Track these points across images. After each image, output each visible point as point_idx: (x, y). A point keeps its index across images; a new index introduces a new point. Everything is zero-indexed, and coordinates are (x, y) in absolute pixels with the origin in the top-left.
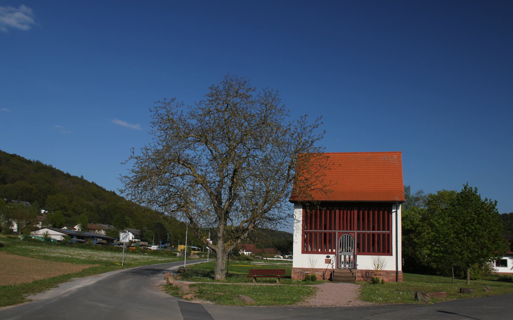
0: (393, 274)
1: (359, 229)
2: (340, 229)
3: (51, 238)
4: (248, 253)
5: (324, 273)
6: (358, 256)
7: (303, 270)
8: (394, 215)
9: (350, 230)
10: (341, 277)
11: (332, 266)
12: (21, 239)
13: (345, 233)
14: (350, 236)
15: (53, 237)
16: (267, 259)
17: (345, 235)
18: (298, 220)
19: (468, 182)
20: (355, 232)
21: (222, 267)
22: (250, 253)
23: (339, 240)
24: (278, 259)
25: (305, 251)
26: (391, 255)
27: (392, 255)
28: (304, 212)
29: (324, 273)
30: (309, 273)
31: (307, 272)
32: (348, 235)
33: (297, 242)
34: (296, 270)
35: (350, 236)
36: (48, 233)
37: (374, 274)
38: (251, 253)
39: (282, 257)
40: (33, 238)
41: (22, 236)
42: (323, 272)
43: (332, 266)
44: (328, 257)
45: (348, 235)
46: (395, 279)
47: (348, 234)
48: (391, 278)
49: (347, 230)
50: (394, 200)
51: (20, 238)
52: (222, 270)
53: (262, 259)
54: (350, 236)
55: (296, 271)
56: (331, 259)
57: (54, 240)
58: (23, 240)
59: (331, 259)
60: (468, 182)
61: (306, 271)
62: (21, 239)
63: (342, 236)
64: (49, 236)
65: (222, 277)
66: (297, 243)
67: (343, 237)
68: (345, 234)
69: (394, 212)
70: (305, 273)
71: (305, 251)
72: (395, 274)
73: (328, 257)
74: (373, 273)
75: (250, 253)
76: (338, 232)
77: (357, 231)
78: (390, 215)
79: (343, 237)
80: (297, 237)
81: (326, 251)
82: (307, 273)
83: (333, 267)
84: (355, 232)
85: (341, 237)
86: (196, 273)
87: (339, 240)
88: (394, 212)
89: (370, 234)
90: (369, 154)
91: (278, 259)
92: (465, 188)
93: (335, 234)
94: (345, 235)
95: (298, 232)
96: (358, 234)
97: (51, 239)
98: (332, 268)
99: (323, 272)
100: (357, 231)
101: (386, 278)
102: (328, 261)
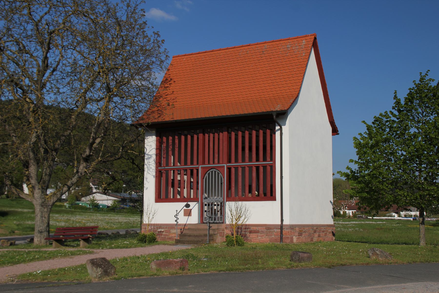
0: (275, 230)
1: (229, 161)
2: (204, 163)
3: (98, 203)
4: (351, 211)
5: (182, 230)
6: (227, 203)
7: (155, 227)
8: (278, 134)
9: (219, 163)
10: (190, 236)
11: (176, 219)
12: (67, 207)
13: (212, 169)
14: (219, 172)
15: (100, 203)
16: (373, 218)
17: (212, 172)
18: (150, 154)
19: (429, 71)
20: (224, 166)
21: (41, 226)
22: (354, 211)
23: (204, 180)
24: (390, 218)
25: (159, 198)
26: (275, 199)
27: (275, 199)
28: (158, 143)
29: (182, 230)
30: (163, 232)
31: (160, 230)
32: (215, 172)
33: (147, 188)
35: (218, 172)
36: (95, 198)
37: (248, 230)
38: (355, 211)
39: (396, 216)
40: (80, 204)
41: (67, 203)
42: (181, 229)
43: (176, 219)
45: (215, 172)
46: (279, 238)
47: (216, 170)
48: (273, 236)
49: (214, 163)
50: (268, 110)
51: (65, 206)
52: (41, 232)
53: (367, 218)
54: (218, 172)
55: (147, 229)
56: (191, 209)
57: (104, 206)
58: (70, 207)
59: (191, 209)
60: (429, 71)
61: (159, 229)
62: (67, 207)
63: (208, 173)
64: (96, 202)
65: (41, 240)
66: (148, 188)
67: (209, 174)
68: (211, 170)
69: (278, 130)
70: (159, 232)
71: (159, 198)
72: (279, 230)
73: (188, 206)
74: (248, 228)
75: (355, 212)
77: (227, 165)
78: (273, 135)
79: (209, 174)
80: (148, 180)
81: (172, 198)
82: (161, 232)
83: (178, 221)
84: (224, 166)
85: (207, 175)
86: (116, 236)
87: (204, 180)
88: (278, 130)
89: (245, 167)
90: (266, 45)
91: (390, 218)
92: (422, 80)
93: (198, 170)
94: (212, 172)
95: (149, 172)
96: (229, 169)
97: (99, 204)
98: (176, 223)
99: (181, 229)
100: (227, 165)
101: (267, 237)
102: (188, 213)
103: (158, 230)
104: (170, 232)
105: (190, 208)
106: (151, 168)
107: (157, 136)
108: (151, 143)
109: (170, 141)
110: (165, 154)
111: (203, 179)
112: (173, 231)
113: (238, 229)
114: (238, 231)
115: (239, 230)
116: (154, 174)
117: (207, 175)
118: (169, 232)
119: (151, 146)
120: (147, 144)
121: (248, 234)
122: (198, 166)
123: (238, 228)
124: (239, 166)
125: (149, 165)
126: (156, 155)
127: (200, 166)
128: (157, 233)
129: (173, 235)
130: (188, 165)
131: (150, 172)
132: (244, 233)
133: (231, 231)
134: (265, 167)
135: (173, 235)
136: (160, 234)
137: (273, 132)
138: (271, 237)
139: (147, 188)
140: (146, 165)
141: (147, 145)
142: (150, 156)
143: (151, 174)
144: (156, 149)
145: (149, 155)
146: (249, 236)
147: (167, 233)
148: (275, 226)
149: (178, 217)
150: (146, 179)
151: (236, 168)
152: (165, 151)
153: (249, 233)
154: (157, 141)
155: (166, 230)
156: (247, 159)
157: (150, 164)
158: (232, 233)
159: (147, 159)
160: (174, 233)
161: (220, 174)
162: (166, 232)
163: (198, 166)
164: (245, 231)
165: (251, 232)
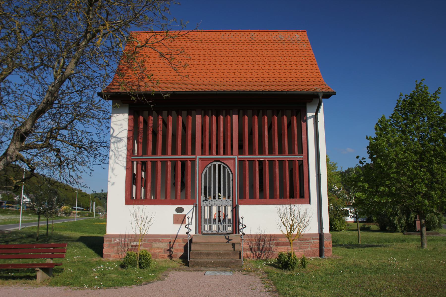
0: (312, 241)
2: (203, 153)
5: (172, 244)
7: (127, 240)
8: (310, 122)
10: (208, 254)
14: (225, 166)
17: (215, 166)
18: (119, 136)
20: (235, 158)
29: (172, 244)
31: (135, 244)
32: (219, 166)
33: (114, 183)
34: (113, 239)
35: (223, 166)
42: (170, 242)
44: (180, 210)
45: (219, 166)
47: (220, 163)
48: (309, 249)
55: (113, 242)
56: (186, 215)
61: (134, 241)
69: (311, 117)
70: (132, 246)
73: (180, 210)
74: (273, 240)
76: (199, 158)
77: (239, 157)
79: (210, 168)
80: (115, 172)
82: (136, 246)
84: (235, 158)
85: (207, 169)
87: (203, 176)
94: (215, 166)
95: (117, 161)
99: (170, 242)
100: (239, 157)
101: (301, 250)
103: (132, 244)
104: (151, 247)
105: (184, 213)
106: (121, 155)
107: (129, 114)
108: (123, 122)
109: (151, 122)
110: (142, 138)
111: (202, 174)
112: (156, 245)
113: (259, 241)
114: (259, 244)
115: (260, 242)
116: (125, 164)
117: (207, 169)
118: (151, 246)
119: (121, 125)
120: (115, 123)
121: (274, 247)
122: (195, 157)
123: (259, 240)
124: (256, 159)
125: (118, 151)
126: (129, 139)
127: (198, 157)
128: (130, 247)
129: (158, 251)
130: (265, 154)
131: (119, 162)
132: (268, 246)
133: (248, 244)
134: (184, 164)
135: (158, 251)
136: (134, 249)
137: (303, 119)
138: (306, 250)
139: (114, 183)
140: (112, 151)
141: (116, 124)
142: (119, 139)
143: (120, 164)
144: (129, 131)
145: (118, 138)
146: (276, 249)
147: (147, 247)
148: (311, 236)
149: (190, 228)
150: (113, 170)
151: (154, 163)
152: (142, 134)
153: (274, 246)
154: (129, 119)
155: (145, 244)
156: (214, 152)
157: (119, 150)
158: (250, 246)
159: (113, 143)
160: (158, 248)
161: (227, 169)
162: (145, 246)
163: (195, 157)
164: (270, 244)
165: (277, 245)
